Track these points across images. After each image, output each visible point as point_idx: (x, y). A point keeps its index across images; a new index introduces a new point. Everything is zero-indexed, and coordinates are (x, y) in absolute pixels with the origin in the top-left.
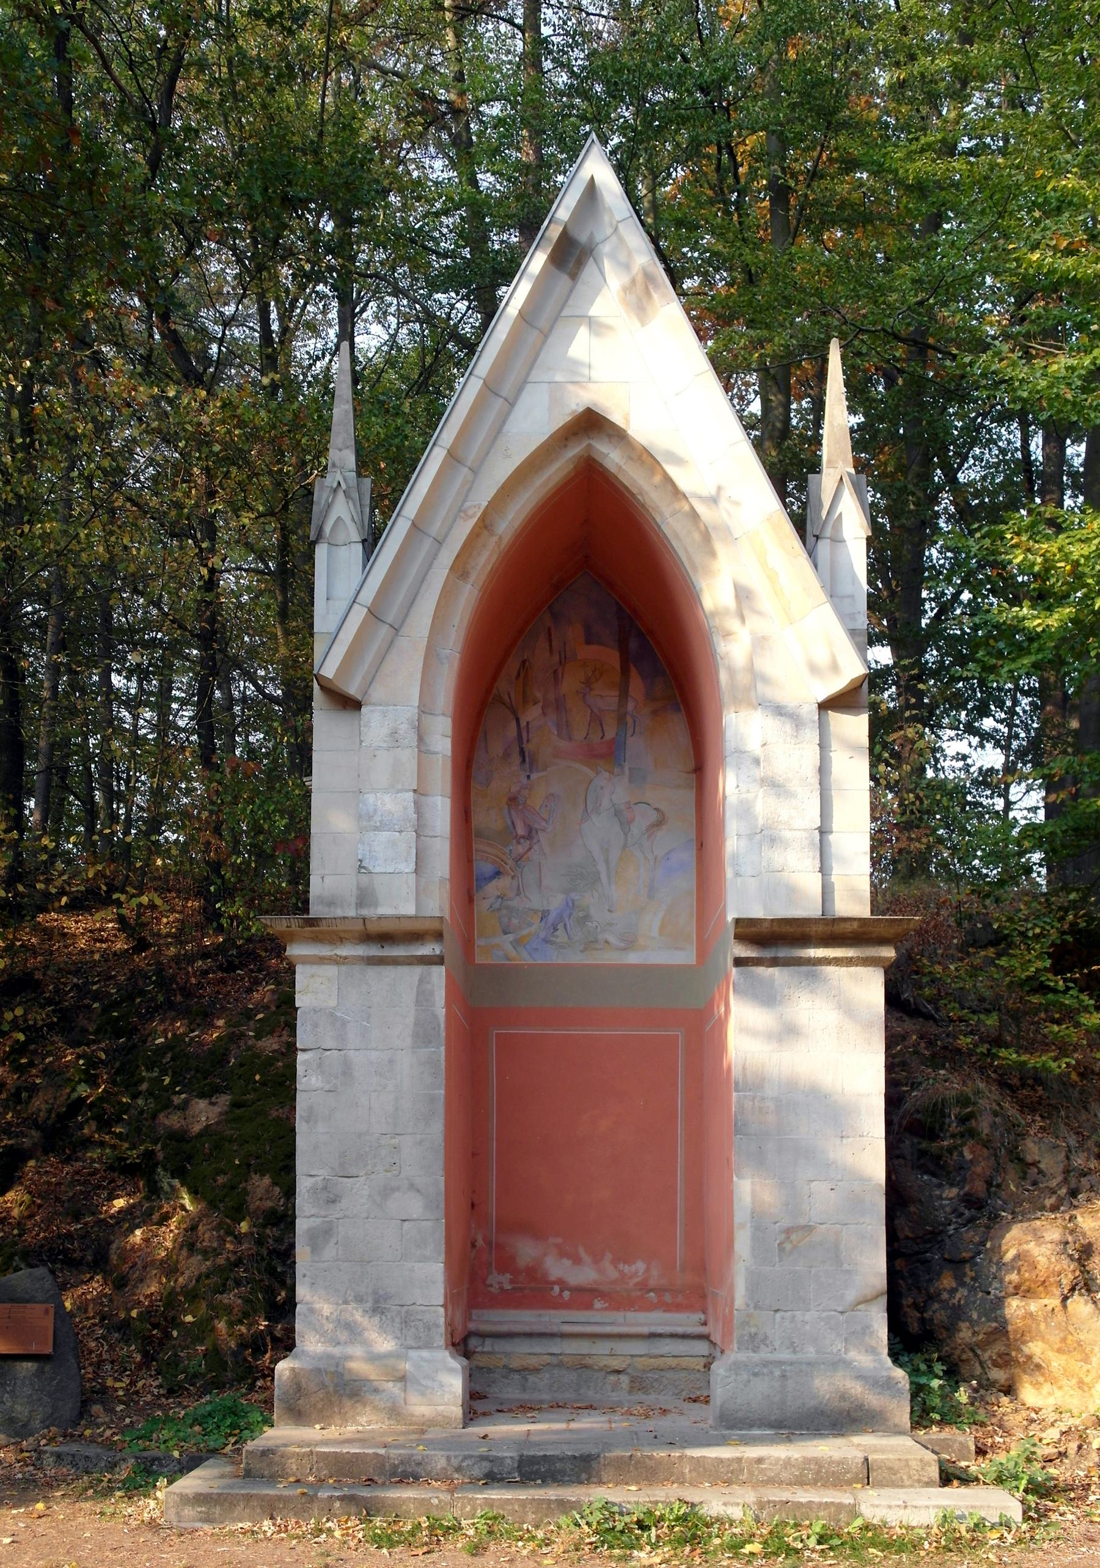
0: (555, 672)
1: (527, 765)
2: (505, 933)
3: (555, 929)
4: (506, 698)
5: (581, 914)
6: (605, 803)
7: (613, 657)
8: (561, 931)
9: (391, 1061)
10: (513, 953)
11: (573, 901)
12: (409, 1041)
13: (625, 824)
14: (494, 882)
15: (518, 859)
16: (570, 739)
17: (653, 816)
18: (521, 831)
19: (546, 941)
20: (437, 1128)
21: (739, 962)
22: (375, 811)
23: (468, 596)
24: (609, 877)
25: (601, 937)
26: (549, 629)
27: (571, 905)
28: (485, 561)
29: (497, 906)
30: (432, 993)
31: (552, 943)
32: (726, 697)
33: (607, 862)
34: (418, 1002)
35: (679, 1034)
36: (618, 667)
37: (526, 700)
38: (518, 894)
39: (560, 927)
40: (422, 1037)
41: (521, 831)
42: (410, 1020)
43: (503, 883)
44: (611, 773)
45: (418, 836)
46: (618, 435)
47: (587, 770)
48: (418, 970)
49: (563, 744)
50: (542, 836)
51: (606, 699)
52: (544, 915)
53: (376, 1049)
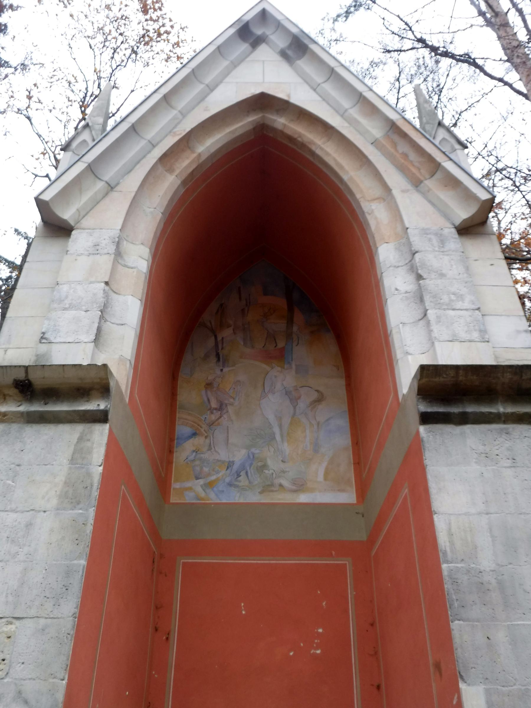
0: (243, 310)
1: (221, 363)
2: (197, 478)
3: (239, 476)
4: (209, 324)
5: (260, 464)
6: (279, 386)
7: (282, 303)
8: (243, 477)
9: (29, 525)
10: (202, 494)
11: (253, 454)
12: (54, 502)
13: (294, 400)
14: (191, 441)
15: (211, 424)
16: (253, 347)
17: (315, 395)
18: (214, 404)
19: (230, 485)
20: (70, 607)
21: (426, 419)
22: (67, 297)
23: (169, 184)
24: (282, 436)
25: (277, 482)
26: (239, 288)
27: (252, 458)
28: (185, 164)
29: (192, 457)
30: (90, 451)
31: (236, 486)
32: (377, 237)
33: (281, 426)
34: (72, 461)
35: (347, 562)
36: (286, 307)
37: (222, 325)
38: (210, 449)
39: (243, 473)
40: (70, 497)
41: (214, 404)
42: (61, 478)
43: (198, 441)
44: (283, 367)
45: (102, 317)
46: (283, 106)
47: (264, 366)
48: (79, 428)
49: (248, 351)
50: (230, 409)
51: (278, 325)
52: (230, 465)
53: (14, 511)
